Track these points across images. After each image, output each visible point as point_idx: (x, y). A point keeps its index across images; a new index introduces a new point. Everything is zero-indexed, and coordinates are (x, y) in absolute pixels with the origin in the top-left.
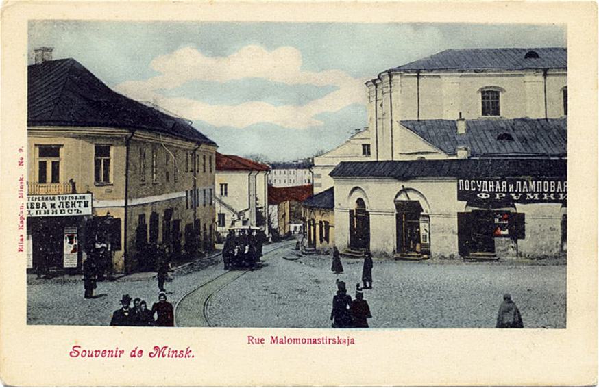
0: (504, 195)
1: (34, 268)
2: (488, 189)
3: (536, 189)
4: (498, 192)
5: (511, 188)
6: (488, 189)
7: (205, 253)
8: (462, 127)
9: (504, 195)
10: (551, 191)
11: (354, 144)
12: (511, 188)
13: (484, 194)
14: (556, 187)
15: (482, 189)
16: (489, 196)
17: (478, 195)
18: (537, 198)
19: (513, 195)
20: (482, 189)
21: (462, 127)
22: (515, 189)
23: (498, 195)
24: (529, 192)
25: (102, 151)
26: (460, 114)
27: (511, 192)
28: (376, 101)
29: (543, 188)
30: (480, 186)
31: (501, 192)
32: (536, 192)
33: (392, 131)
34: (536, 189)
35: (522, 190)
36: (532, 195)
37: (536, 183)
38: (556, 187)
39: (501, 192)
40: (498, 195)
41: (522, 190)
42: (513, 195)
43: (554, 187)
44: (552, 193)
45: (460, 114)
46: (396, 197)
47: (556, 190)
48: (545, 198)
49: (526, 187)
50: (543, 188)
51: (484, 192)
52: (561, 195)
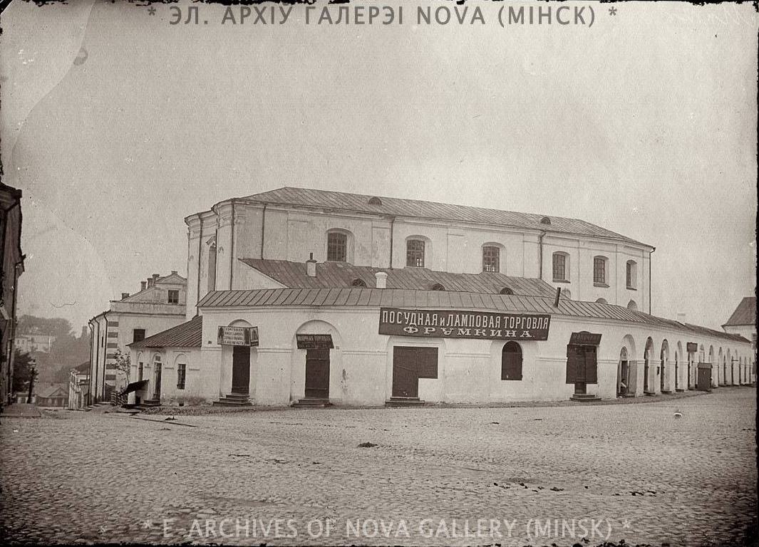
0: (434, 330)
1: (19, 357)
2: (417, 322)
3: (468, 324)
4: (427, 326)
5: (442, 321)
6: (417, 322)
7: (520, 534)
8: (312, 270)
9: (434, 330)
10: (484, 326)
11: (159, 289)
12: (442, 321)
13: (411, 328)
14: (424, 319)
15: (409, 322)
16: (417, 330)
17: (405, 329)
18: (468, 334)
19: (444, 330)
20: (409, 322)
21: (312, 270)
22: (446, 323)
23: (427, 329)
24: (460, 327)
25: (725, 381)
26: (311, 254)
27: (442, 327)
28: (201, 237)
29: (475, 323)
30: (408, 319)
31: (431, 326)
32: (468, 327)
33: (232, 276)
34: (468, 324)
35: (454, 323)
36: (464, 330)
37: (469, 317)
38: (424, 319)
39: (431, 326)
40: (427, 329)
41: (454, 323)
42: (444, 330)
43: (486, 322)
44: (484, 328)
45: (311, 254)
46: (298, 330)
47: (488, 325)
48: (493, 335)
49: (429, 320)
50: (475, 323)
51: (411, 326)
52: (493, 331)
